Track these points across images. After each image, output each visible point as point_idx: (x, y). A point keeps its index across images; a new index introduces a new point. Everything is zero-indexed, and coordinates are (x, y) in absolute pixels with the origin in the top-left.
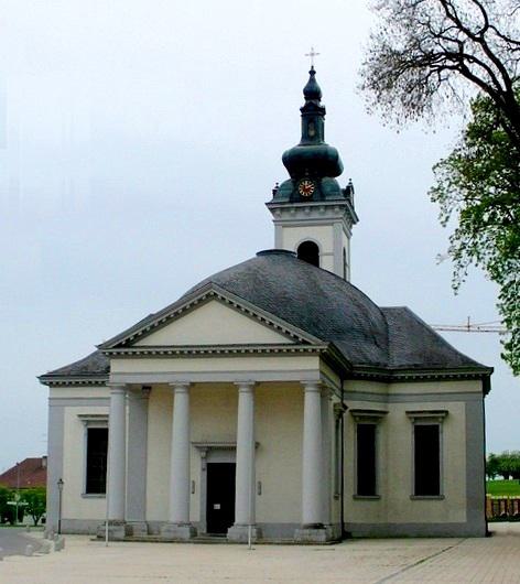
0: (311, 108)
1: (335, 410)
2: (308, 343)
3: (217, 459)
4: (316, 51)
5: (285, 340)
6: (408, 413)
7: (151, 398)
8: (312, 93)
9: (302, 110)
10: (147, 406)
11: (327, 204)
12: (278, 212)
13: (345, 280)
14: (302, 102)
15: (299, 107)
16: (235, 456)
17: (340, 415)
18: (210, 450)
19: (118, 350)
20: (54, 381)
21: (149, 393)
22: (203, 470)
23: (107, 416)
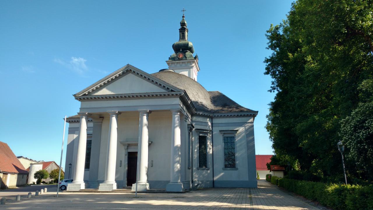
0: (183, 29)
1: (188, 127)
2: (174, 91)
3: (131, 150)
4: (184, 9)
5: (164, 91)
6: (220, 131)
7: (103, 122)
8: (183, 24)
9: (179, 30)
10: (101, 126)
11: (188, 61)
12: (170, 64)
13: (209, 209)
14: (180, 27)
15: (179, 29)
16: (137, 149)
17: (191, 130)
18: (129, 146)
19: (84, 97)
20: (71, 120)
21: (103, 120)
22: (126, 155)
23: (91, 134)
